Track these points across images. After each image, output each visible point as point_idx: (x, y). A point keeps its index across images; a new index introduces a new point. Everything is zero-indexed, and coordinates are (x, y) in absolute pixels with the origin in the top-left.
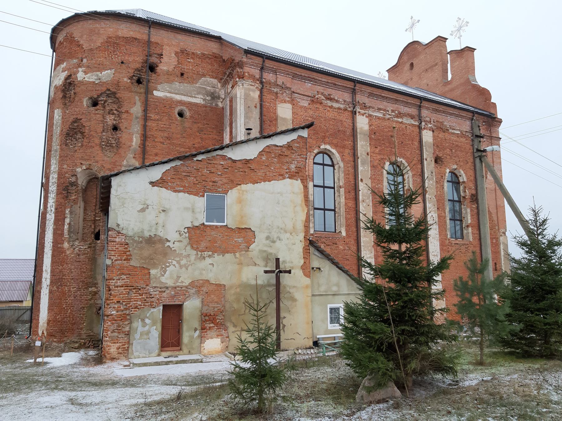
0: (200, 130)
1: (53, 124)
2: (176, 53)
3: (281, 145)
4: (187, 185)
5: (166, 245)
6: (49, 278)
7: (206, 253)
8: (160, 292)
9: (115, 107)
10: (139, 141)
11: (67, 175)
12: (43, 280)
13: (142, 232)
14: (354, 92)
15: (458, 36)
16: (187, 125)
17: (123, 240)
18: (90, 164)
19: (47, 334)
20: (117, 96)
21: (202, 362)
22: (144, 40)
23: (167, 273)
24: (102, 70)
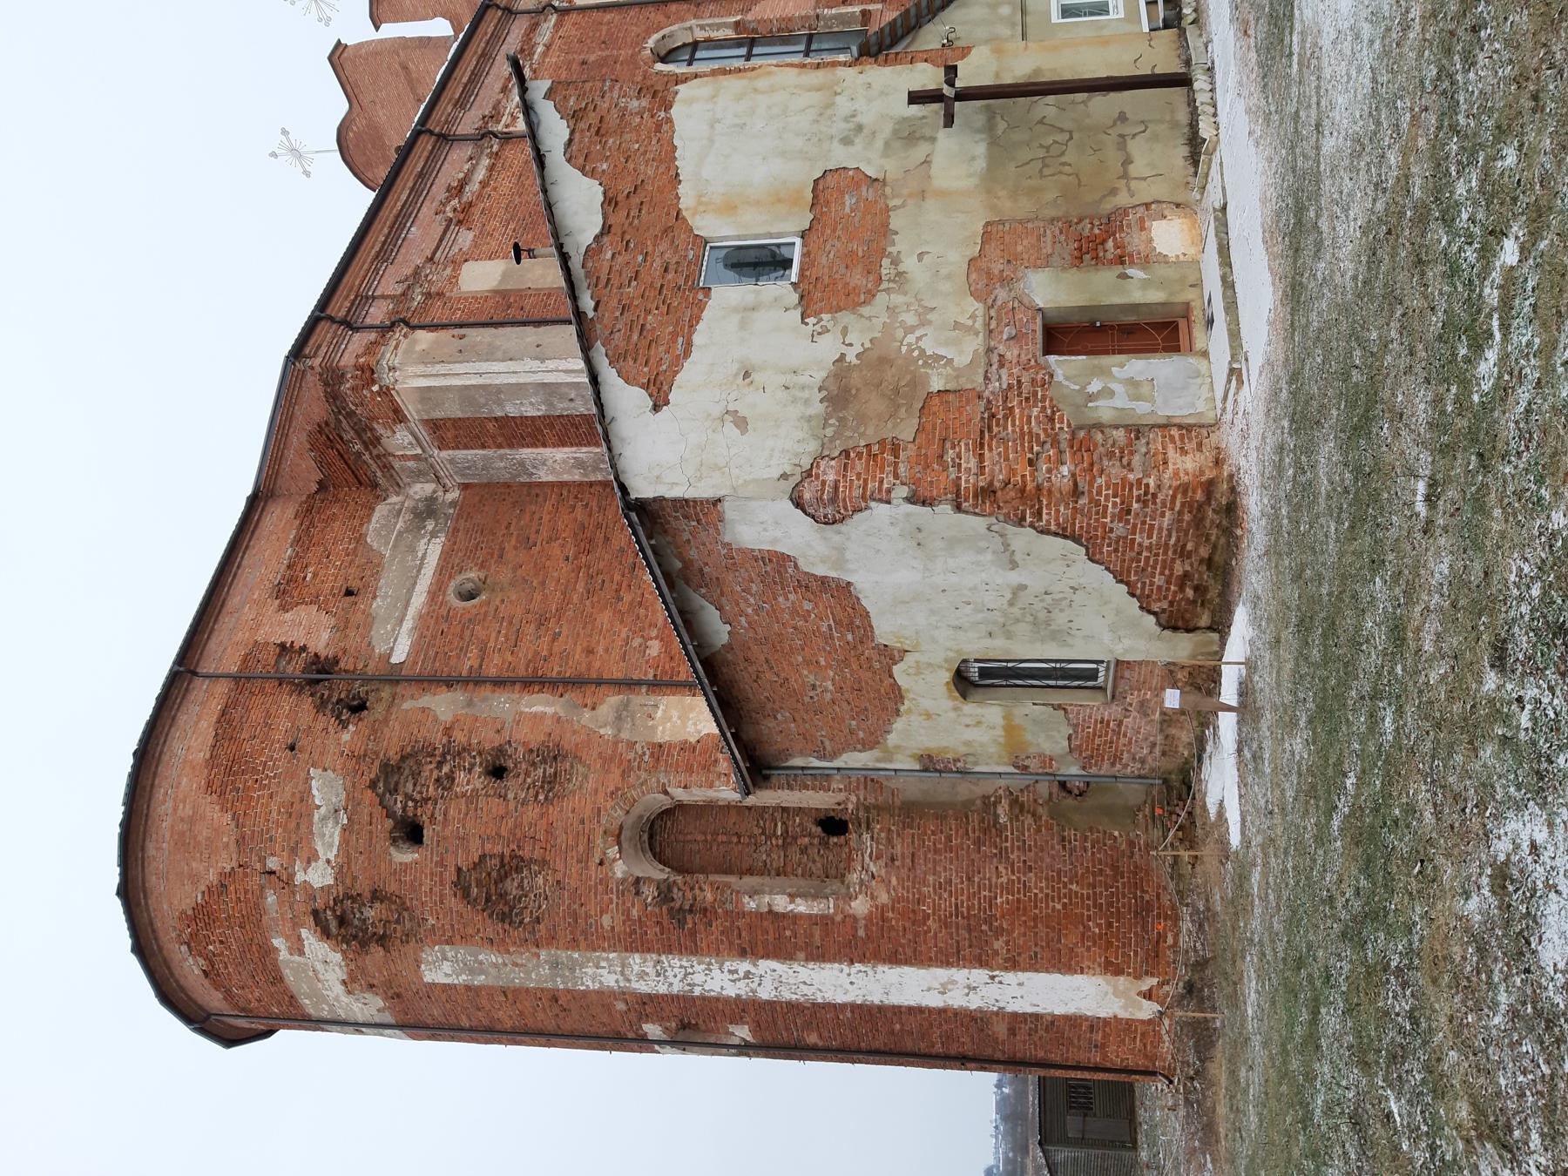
0: (527, 543)
1: (468, 988)
2: (284, 608)
3: (567, 131)
5: (855, 361)
6: (966, 971)
7: (884, 272)
8: (1002, 365)
9: (431, 771)
11: (635, 913)
12: (974, 1003)
13: (809, 419)
14: (445, 139)
16: (504, 575)
18: (605, 832)
19: (1153, 975)
20: (394, 758)
21: (1224, 208)
22: (231, 690)
23: (942, 352)
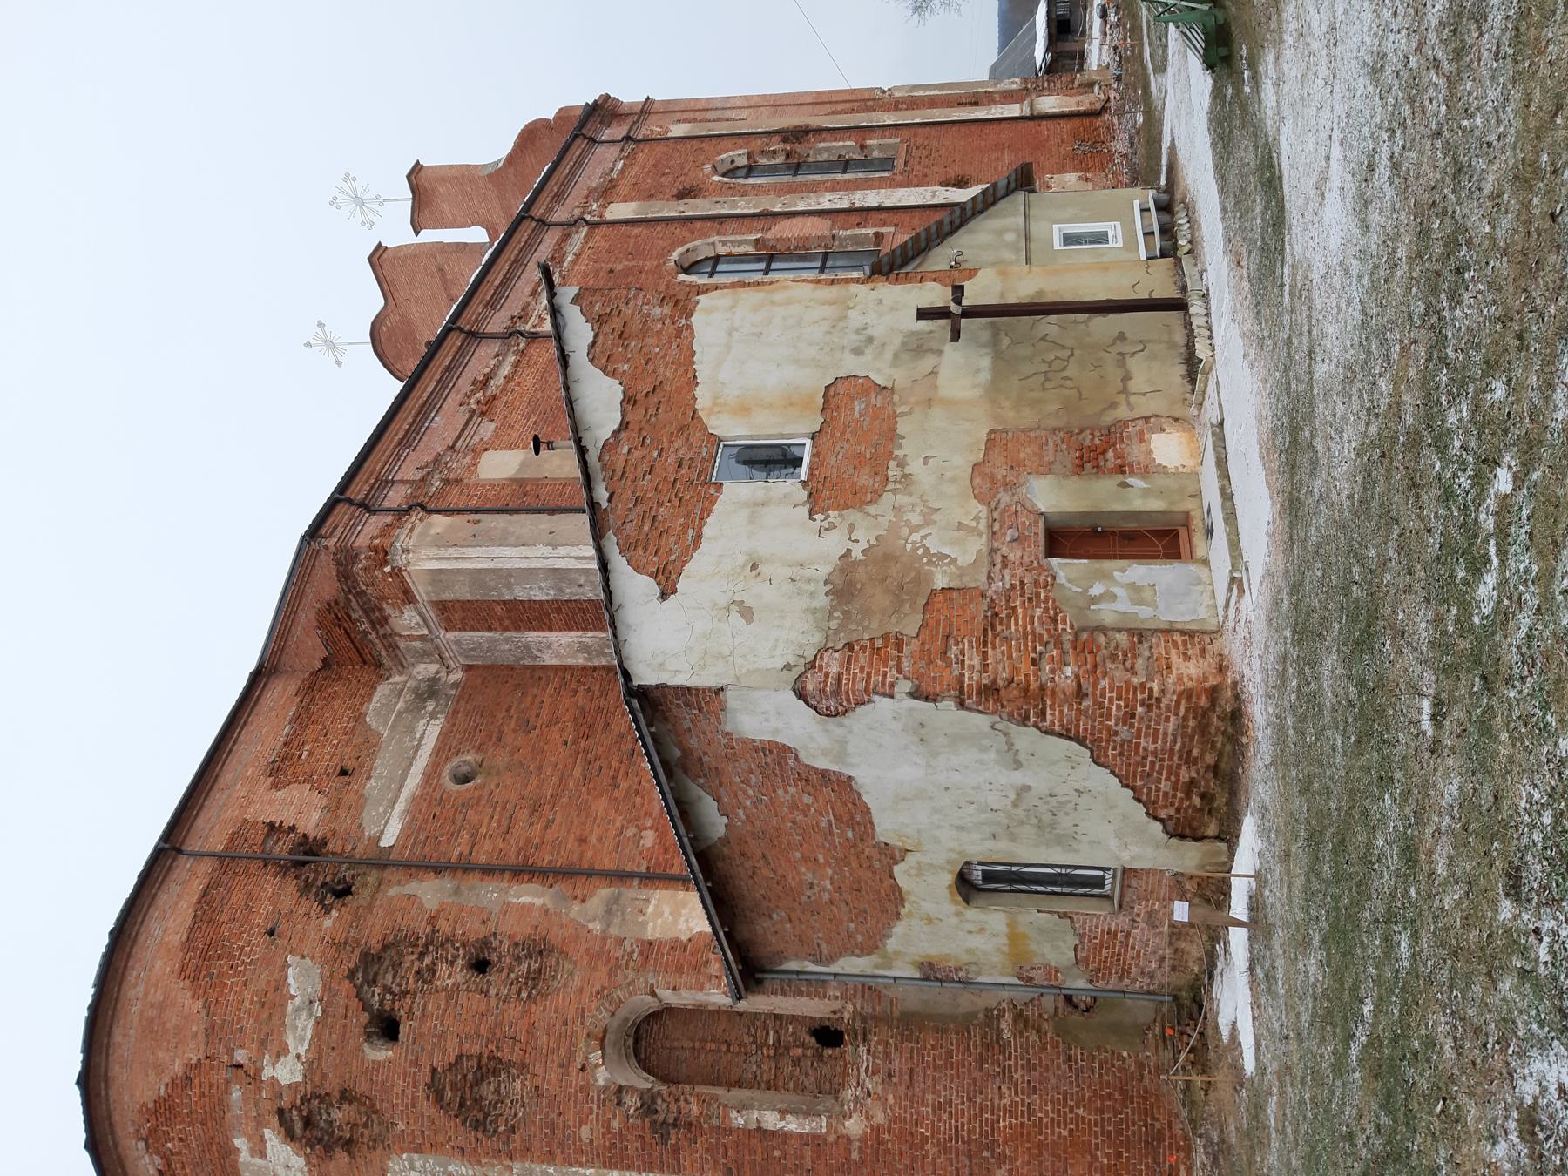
0: (526, 726)
2: (276, 786)
4: (682, 520)
7: (890, 473)
8: (1005, 566)
9: (412, 962)
10: (535, 886)
11: (615, 1124)
13: (814, 611)
15: (376, 207)
16: (501, 759)
17: (837, 655)
18: (588, 1035)
21: (1221, 424)
22: (214, 870)
24: (282, 996)
